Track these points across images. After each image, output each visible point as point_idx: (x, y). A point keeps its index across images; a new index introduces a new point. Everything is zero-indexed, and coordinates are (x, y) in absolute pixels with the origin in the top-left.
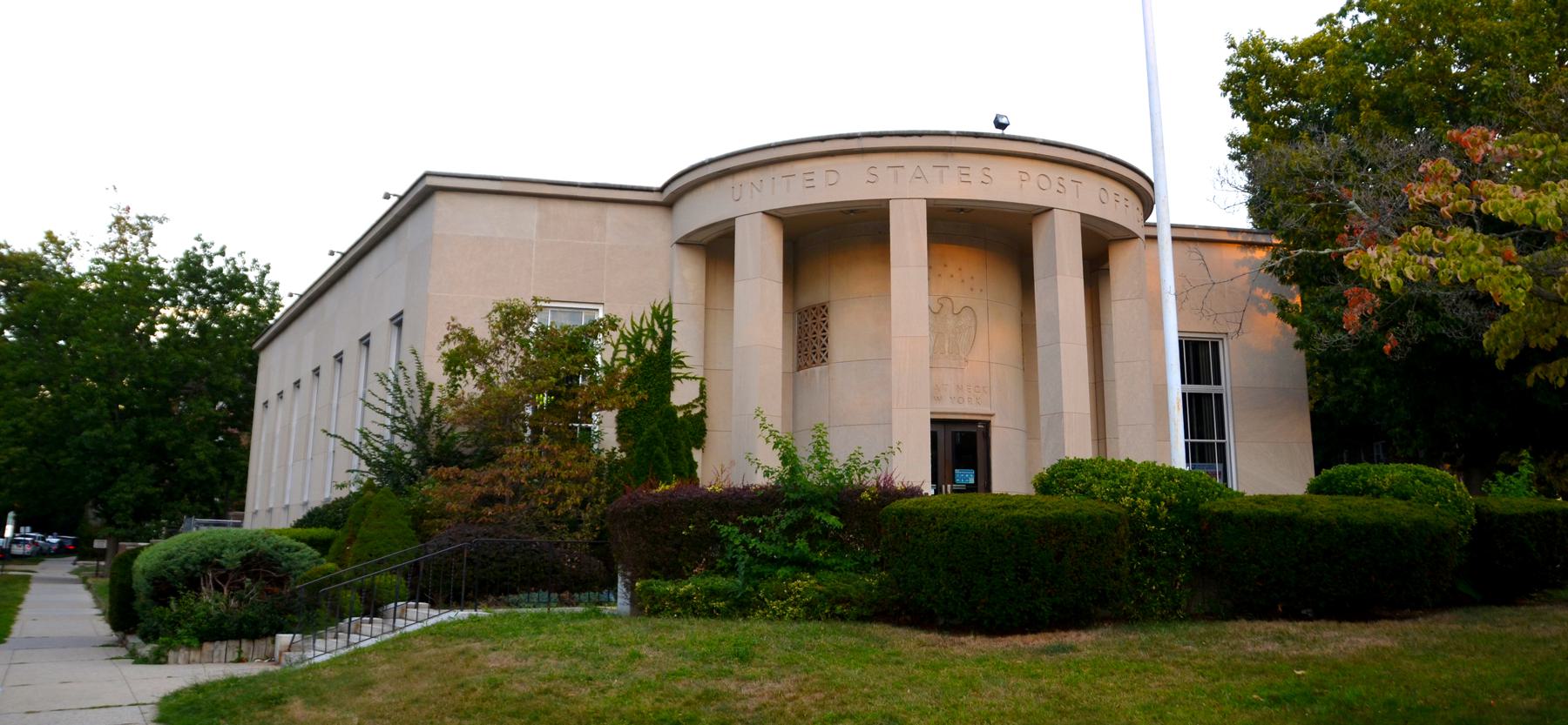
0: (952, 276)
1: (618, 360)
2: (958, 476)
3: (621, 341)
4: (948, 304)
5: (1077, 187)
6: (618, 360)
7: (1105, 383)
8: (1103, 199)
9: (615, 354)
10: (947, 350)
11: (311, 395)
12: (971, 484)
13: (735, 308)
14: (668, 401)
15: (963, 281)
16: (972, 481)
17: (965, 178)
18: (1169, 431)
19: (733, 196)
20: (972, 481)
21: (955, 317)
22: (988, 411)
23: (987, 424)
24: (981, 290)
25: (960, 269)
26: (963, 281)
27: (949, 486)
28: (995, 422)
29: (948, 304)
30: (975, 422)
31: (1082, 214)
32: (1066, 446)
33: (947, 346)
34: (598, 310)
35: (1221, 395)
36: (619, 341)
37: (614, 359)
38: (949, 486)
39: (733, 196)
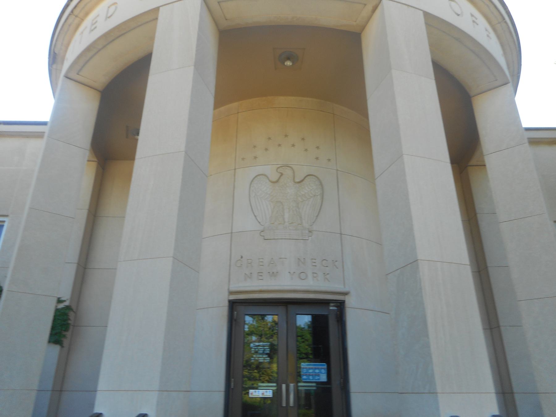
0: (293, 145)
2: (305, 371)
4: (288, 172)
7: (490, 270)
10: (286, 220)
11: (56, 41)
12: (322, 383)
15: (306, 150)
16: (323, 378)
17: (260, 278)
19: (116, 8)
20: (323, 378)
22: (338, 287)
23: (341, 305)
25: (303, 139)
26: (306, 150)
27: (292, 385)
28: (351, 302)
29: (288, 172)
30: (325, 303)
31: (427, 15)
32: (430, 320)
33: (286, 216)
34: (4, 222)
38: (292, 385)
39: (116, 8)
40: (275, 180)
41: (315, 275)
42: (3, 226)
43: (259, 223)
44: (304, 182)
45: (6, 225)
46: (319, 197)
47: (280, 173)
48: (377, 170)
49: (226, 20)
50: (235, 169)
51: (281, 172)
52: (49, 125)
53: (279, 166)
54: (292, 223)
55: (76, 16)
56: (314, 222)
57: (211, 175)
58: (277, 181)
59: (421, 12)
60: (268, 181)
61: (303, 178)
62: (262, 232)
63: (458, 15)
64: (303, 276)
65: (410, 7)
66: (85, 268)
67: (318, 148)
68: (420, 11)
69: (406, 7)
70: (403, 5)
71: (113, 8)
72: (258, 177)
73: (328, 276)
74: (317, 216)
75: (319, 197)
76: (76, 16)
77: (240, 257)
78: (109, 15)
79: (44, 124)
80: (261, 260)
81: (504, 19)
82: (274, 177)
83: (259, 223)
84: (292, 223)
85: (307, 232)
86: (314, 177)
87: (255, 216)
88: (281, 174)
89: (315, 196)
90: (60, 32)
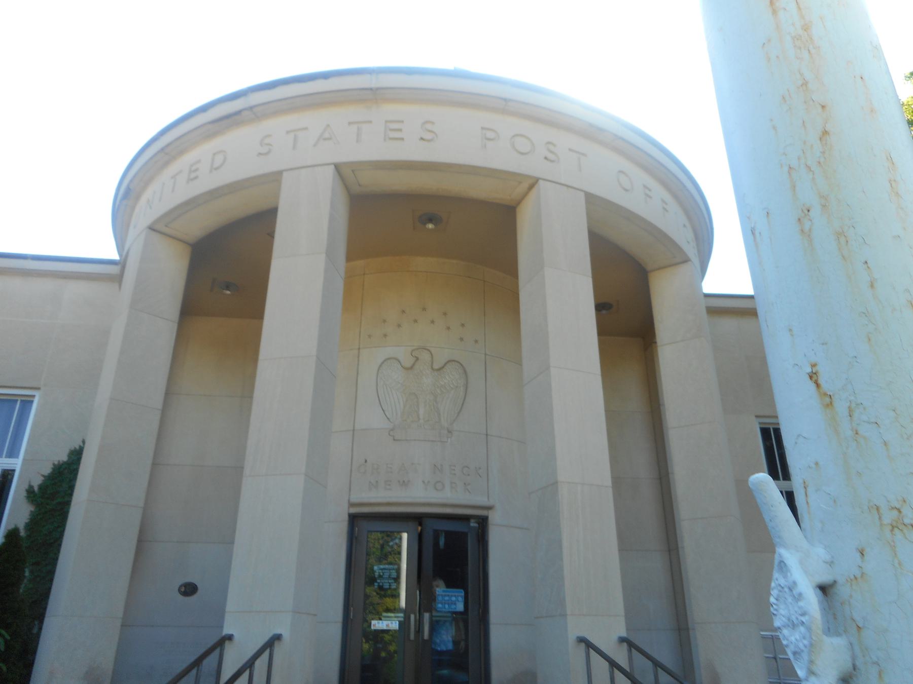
0: (433, 322)
4: (425, 356)
10: (421, 417)
17: (388, 487)
29: (425, 356)
33: (421, 411)
34: (34, 396)
42: (32, 402)
47: (416, 357)
51: (417, 356)
53: (415, 348)
58: (412, 368)
89: (457, 387)
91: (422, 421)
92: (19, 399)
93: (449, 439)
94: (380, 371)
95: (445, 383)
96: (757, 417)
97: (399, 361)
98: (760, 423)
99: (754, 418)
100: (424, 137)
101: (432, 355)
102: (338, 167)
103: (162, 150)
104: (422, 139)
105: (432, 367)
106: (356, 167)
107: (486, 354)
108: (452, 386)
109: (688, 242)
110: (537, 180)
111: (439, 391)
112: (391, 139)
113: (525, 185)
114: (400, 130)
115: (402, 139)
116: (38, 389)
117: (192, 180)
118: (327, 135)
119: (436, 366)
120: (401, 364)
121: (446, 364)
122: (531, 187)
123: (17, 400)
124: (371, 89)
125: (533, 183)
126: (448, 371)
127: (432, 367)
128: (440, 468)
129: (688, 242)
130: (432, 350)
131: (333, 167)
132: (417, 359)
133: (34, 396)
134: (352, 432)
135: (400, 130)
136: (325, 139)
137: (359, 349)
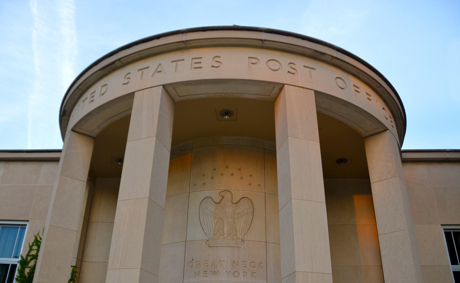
0: (232, 175)
1: (30, 256)
3: (35, 244)
4: (228, 195)
5: (311, 71)
6: (30, 256)
8: (342, 87)
9: (29, 252)
10: (225, 232)
11: (67, 103)
13: (115, 222)
14: (29, 272)
17: (206, 275)
18: (65, 133)
21: (234, 205)
24: (259, 185)
25: (240, 169)
29: (228, 195)
33: (226, 229)
34: (26, 225)
35: (452, 264)
36: (33, 243)
37: (28, 255)
40: (217, 201)
41: (245, 274)
42: (25, 228)
43: (206, 234)
44: (239, 203)
45: (27, 227)
46: (250, 214)
47: (222, 196)
48: (280, 206)
49: (180, 96)
50: (189, 192)
51: (222, 195)
52: (63, 152)
53: (221, 191)
54: (230, 234)
55: (80, 89)
56: (246, 234)
57: (172, 196)
58: (220, 203)
59: (314, 91)
60: (213, 202)
61: (238, 201)
62: (208, 241)
63: (343, 89)
64: (236, 274)
65: (305, 89)
66: (82, 261)
67: (251, 176)
68: (312, 91)
69: (302, 88)
70: (300, 88)
71: (105, 87)
72: (206, 199)
73: (255, 274)
74: (248, 229)
75: (250, 214)
76: (80, 89)
77: (192, 259)
78: (102, 93)
79: (59, 151)
80: (206, 262)
81: (381, 85)
82: (218, 199)
83: (206, 234)
84: (230, 234)
85: (240, 241)
86: (247, 199)
87: (203, 229)
88: (222, 197)
89: (247, 213)
90: (73, 93)
91: (226, 235)
92: (20, 227)
93: (242, 245)
94: (201, 205)
95: (240, 211)
96: (442, 225)
97: (213, 200)
98: (444, 229)
99: (440, 225)
100: (214, 65)
101: (232, 195)
102: (164, 86)
103: (78, 87)
104: (213, 66)
105: (232, 202)
106: (175, 85)
107: (265, 193)
108: (244, 213)
109: (387, 119)
110: (284, 85)
111: (236, 216)
112: (195, 68)
113: (277, 89)
114: (200, 63)
115: (201, 67)
116: (28, 221)
117: (91, 102)
118: (159, 70)
119: (234, 202)
120: (213, 201)
121: (240, 200)
122: (281, 89)
123: (19, 227)
124: (183, 42)
125: (281, 87)
126: (242, 204)
127: (232, 202)
128: (236, 263)
129: (387, 119)
130: (232, 191)
131: (162, 86)
132: (223, 197)
133: (26, 225)
134: (185, 242)
135: (200, 63)
136: (158, 72)
137: (189, 192)
